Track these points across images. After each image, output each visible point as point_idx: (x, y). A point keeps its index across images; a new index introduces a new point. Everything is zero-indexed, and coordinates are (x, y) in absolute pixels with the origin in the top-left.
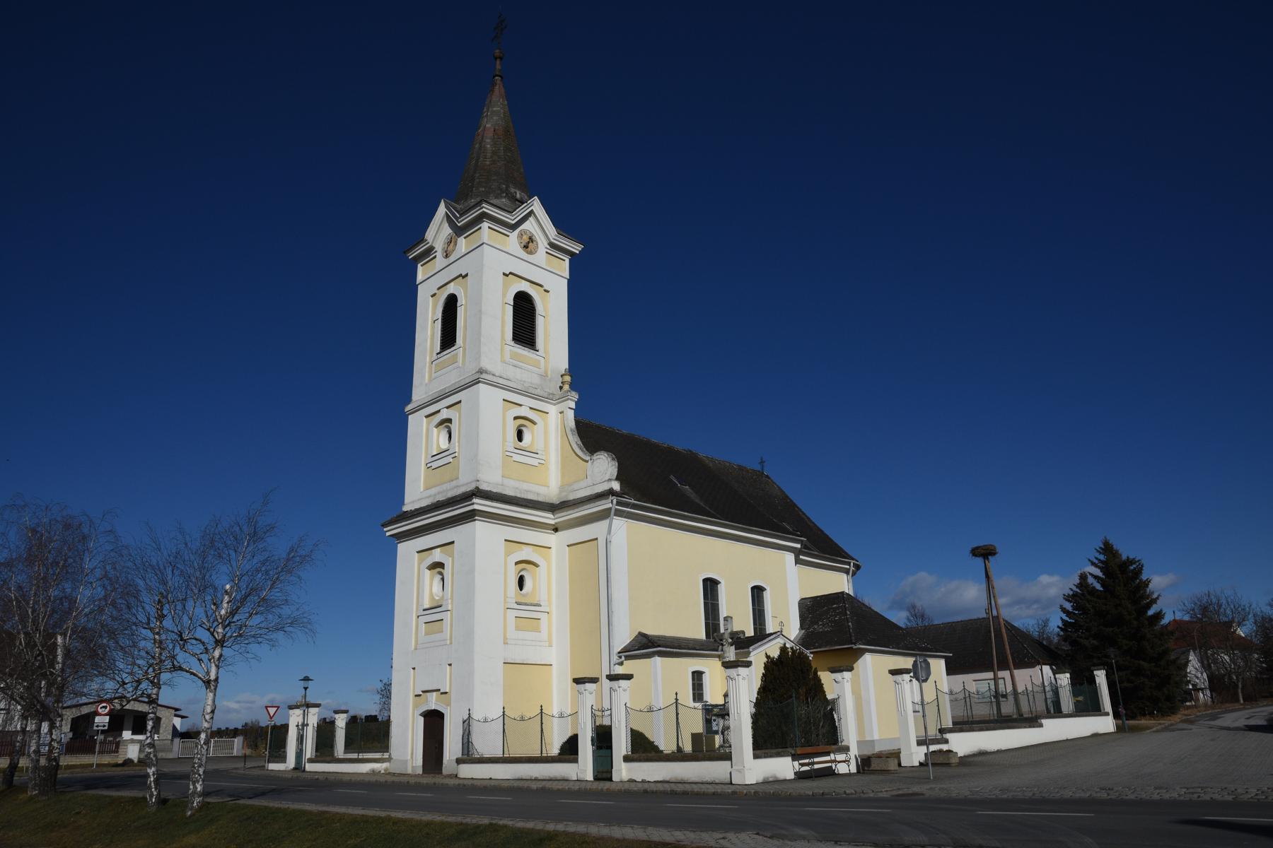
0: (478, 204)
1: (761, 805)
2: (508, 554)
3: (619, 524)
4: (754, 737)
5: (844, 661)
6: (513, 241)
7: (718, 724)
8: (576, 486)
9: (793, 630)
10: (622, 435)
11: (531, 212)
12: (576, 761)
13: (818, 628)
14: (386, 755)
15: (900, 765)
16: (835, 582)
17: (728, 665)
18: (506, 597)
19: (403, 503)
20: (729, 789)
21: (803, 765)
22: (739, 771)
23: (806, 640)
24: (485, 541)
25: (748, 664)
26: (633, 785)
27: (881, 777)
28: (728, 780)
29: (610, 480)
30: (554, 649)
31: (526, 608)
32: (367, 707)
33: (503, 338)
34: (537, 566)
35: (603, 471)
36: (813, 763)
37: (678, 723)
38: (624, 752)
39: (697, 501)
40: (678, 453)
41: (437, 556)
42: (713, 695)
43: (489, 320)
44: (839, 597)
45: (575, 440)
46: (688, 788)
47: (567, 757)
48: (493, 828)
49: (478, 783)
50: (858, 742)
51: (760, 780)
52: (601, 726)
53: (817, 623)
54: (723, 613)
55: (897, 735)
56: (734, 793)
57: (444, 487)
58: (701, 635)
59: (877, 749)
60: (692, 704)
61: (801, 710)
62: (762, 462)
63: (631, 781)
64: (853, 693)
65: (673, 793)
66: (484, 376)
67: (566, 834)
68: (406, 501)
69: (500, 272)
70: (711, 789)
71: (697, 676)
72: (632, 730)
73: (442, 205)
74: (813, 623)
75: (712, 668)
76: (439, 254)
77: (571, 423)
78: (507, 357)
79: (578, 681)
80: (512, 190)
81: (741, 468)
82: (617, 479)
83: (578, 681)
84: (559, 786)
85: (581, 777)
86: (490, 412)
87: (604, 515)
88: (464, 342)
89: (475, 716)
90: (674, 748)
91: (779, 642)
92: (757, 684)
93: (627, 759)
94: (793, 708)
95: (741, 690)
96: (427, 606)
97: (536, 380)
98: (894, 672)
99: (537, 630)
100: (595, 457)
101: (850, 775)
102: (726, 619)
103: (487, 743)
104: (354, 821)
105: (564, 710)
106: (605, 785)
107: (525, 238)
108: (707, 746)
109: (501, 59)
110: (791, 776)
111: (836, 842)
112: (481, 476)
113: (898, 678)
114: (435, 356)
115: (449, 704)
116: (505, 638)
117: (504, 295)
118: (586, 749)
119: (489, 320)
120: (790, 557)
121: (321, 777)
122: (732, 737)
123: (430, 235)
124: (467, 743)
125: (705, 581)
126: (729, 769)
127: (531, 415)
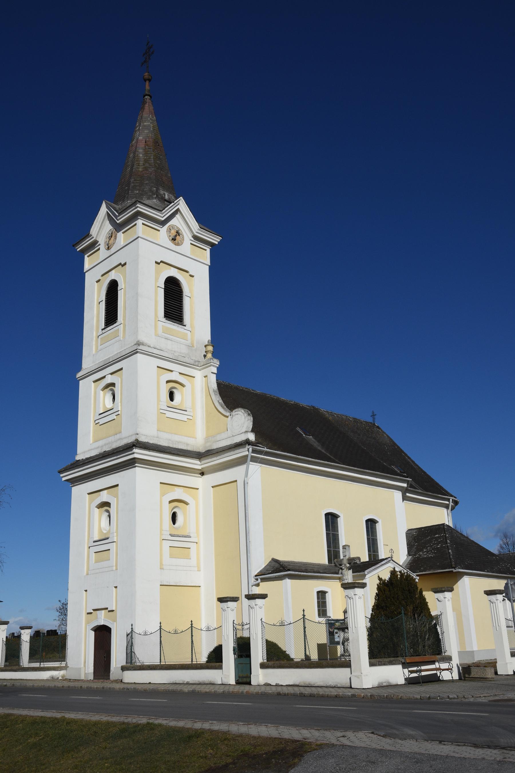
0: (134, 204)
1: (375, 707)
2: (163, 494)
3: (254, 468)
4: (370, 647)
5: (446, 583)
6: (163, 234)
7: (339, 637)
8: (218, 437)
9: (402, 556)
10: (256, 395)
11: (178, 210)
12: (220, 668)
13: (423, 554)
14: (63, 664)
15: (496, 673)
16: (436, 515)
17: (346, 586)
18: (161, 530)
19: (76, 453)
20: (349, 692)
21: (412, 672)
22: (358, 677)
23: (413, 565)
24: (142, 483)
25: (363, 586)
26: (268, 688)
27: (480, 684)
28: (348, 685)
29: (246, 432)
30: (202, 573)
31: (178, 539)
32: (48, 623)
33: (156, 315)
34: (186, 503)
35: (240, 424)
36: (421, 671)
37: (305, 636)
38: (260, 660)
39: (319, 448)
40: (303, 408)
41: (104, 497)
42: (335, 612)
43: (144, 301)
44: (441, 528)
45: (217, 399)
46: (314, 691)
47: (213, 664)
48: (150, 727)
49: (139, 687)
50: (459, 652)
51: (376, 684)
52: (241, 638)
53: (422, 550)
54: (342, 542)
55: (494, 648)
56: (353, 696)
57: (110, 439)
58: (325, 561)
59: (477, 658)
60: (317, 619)
61: (408, 625)
62: (373, 415)
63: (267, 685)
64: (454, 610)
65: (302, 695)
66: (141, 347)
67: (211, 731)
68: (79, 451)
69: (152, 258)
70: (334, 692)
71: (322, 595)
72: (267, 641)
73: (104, 206)
74: (419, 550)
75: (332, 588)
76: (102, 247)
77: (214, 385)
78: (160, 331)
79: (221, 600)
80: (162, 192)
81: (356, 420)
82: (253, 431)
83: (221, 600)
84: (207, 689)
85: (225, 681)
86: (146, 377)
87: (242, 461)
88: (124, 319)
89: (136, 630)
90: (303, 657)
91: (390, 566)
92: (371, 602)
93: (263, 666)
94: (402, 623)
95: (358, 607)
96: (96, 539)
97: (184, 350)
98: (489, 593)
99: (188, 557)
100: (234, 412)
101: (453, 681)
102: (344, 547)
103: (146, 654)
104: (35, 722)
105: (212, 626)
106: (245, 688)
107: (173, 232)
108: (330, 656)
109: (150, 80)
110: (402, 681)
111: (440, 742)
112: (140, 430)
113: (493, 597)
114: (100, 332)
115: (115, 620)
116: (161, 564)
117: (157, 279)
118: (229, 658)
119: (144, 301)
120: (398, 495)
121: (9, 684)
122: (351, 647)
123: (94, 231)
124: (130, 653)
125: (327, 515)
126: (349, 675)
127: (181, 379)
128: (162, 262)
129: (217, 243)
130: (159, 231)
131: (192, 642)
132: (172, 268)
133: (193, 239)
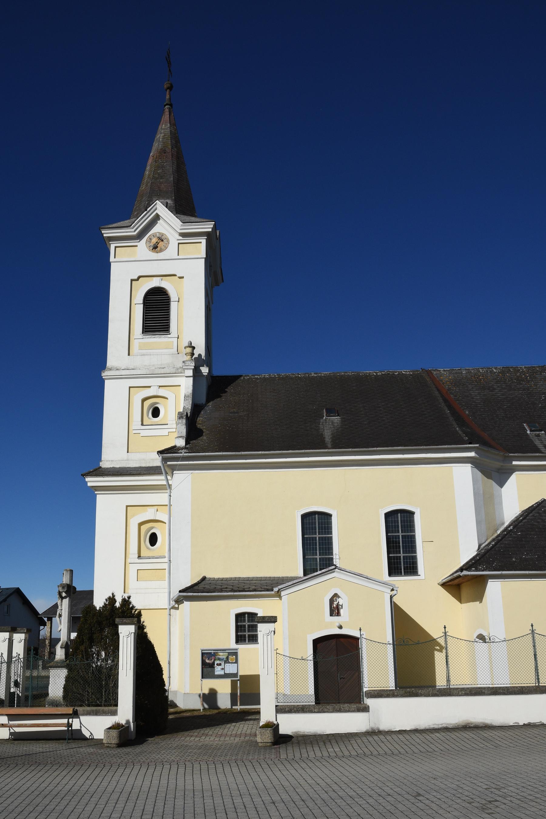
127: (162, 392)
128: (139, 277)
129: (210, 230)
130: (137, 246)
131: (535, 655)
132: (154, 278)
133: (181, 238)
